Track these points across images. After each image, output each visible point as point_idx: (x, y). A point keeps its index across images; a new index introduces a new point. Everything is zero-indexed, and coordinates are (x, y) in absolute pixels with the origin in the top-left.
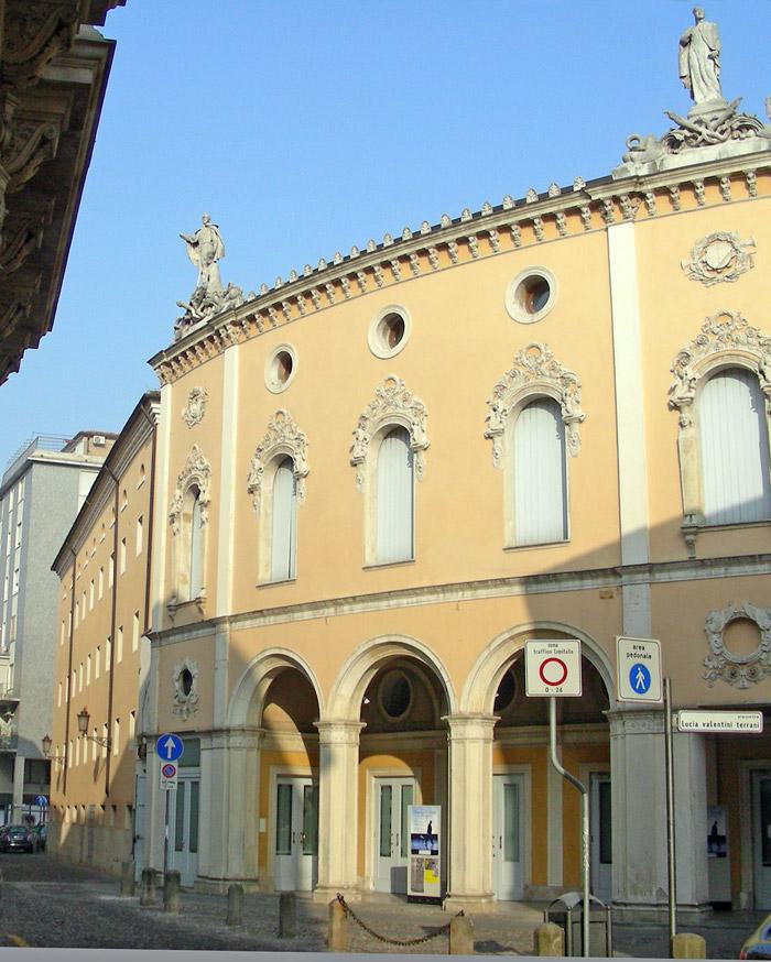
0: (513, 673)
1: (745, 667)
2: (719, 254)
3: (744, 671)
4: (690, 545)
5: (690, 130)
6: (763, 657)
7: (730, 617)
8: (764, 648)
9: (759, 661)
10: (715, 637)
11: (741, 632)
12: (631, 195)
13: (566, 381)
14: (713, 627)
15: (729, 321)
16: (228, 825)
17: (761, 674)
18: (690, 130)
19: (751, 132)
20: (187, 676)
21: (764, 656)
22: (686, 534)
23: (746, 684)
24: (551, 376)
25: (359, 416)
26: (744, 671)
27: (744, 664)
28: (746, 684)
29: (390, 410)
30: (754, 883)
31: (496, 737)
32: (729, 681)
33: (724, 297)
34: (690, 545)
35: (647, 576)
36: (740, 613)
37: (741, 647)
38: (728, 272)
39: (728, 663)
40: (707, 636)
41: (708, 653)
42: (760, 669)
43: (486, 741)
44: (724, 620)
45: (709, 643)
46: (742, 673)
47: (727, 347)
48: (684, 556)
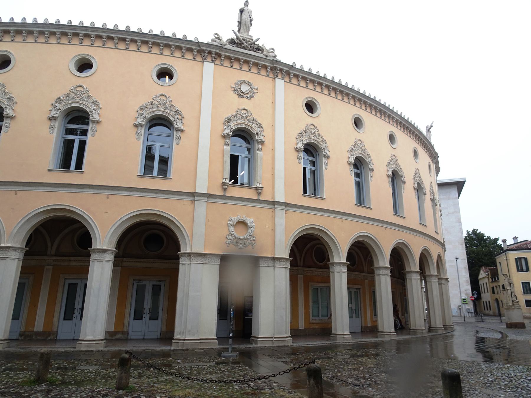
0: (76, 226)
2: (245, 88)
4: (225, 190)
5: (240, 41)
7: (238, 220)
9: (248, 238)
12: (287, 71)
13: (95, 103)
15: (246, 112)
18: (240, 41)
19: (260, 52)
22: (223, 185)
24: (170, 110)
25: (184, 117)
29: (78, 100)
31: (24, 260)
33: (245, 103)
34: (225, 190)
35: (206, 199)
38: (247, 95)
42: (247, 242)
43: (19, 260)
44: (236, 222)
47: (244, 121)
48: (256, 197)
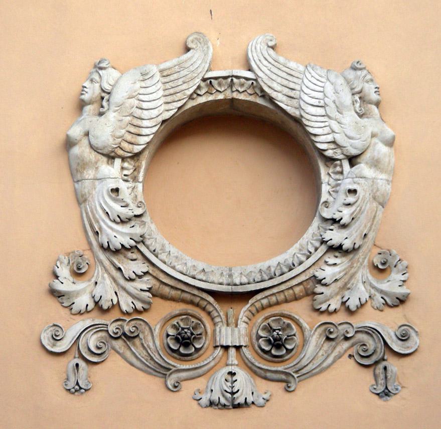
1: (243, 311)
3: (236, 329)
6: (328, 273)
8: (335, 236)
9: (311, 288)
10: (112, 172)
11: (227, 170)
14: (107, 129)
16: (73, 339)
17: (315, 340)
20: (62, 283)
21: (332, 269)
23: (245, 385)
26: (236, 329)
27: (245, 297)
28: (245, 385)
30: (298, 78)
32: (163, 371)
36: (230, 80)
37: (223, 224)
39: (170, 289)
40: (76, 170)
41: (80, 246)
44: (158, 108)
45: (81, 200)
46: (227, 336)
